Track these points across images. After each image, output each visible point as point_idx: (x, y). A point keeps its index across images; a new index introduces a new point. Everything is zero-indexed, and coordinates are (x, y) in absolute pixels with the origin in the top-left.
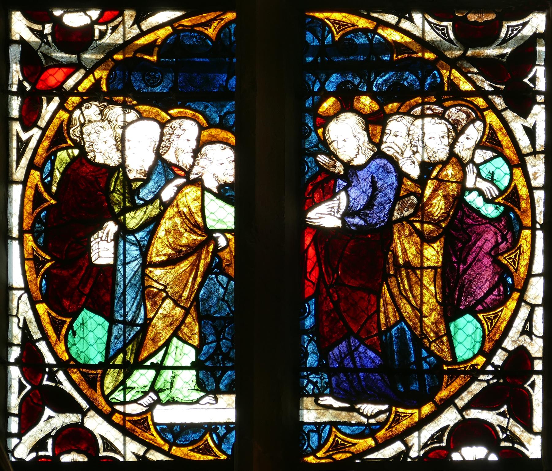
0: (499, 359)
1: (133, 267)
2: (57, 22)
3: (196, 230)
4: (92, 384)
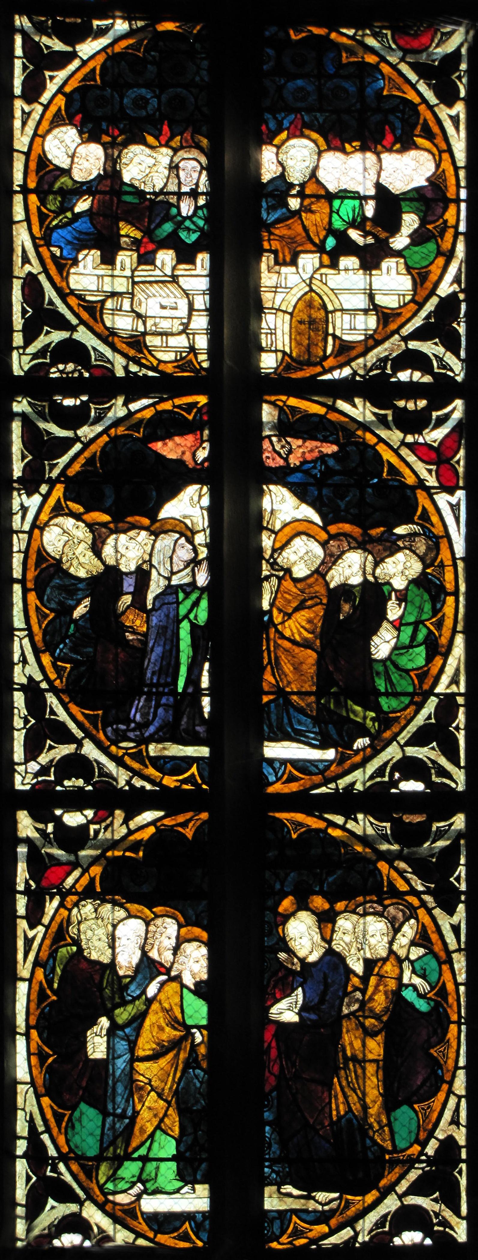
0: (430, 1150)
1: (121, 1064)
2: (58, 821)
3: (176, 1025)
4: (89, 1176)
